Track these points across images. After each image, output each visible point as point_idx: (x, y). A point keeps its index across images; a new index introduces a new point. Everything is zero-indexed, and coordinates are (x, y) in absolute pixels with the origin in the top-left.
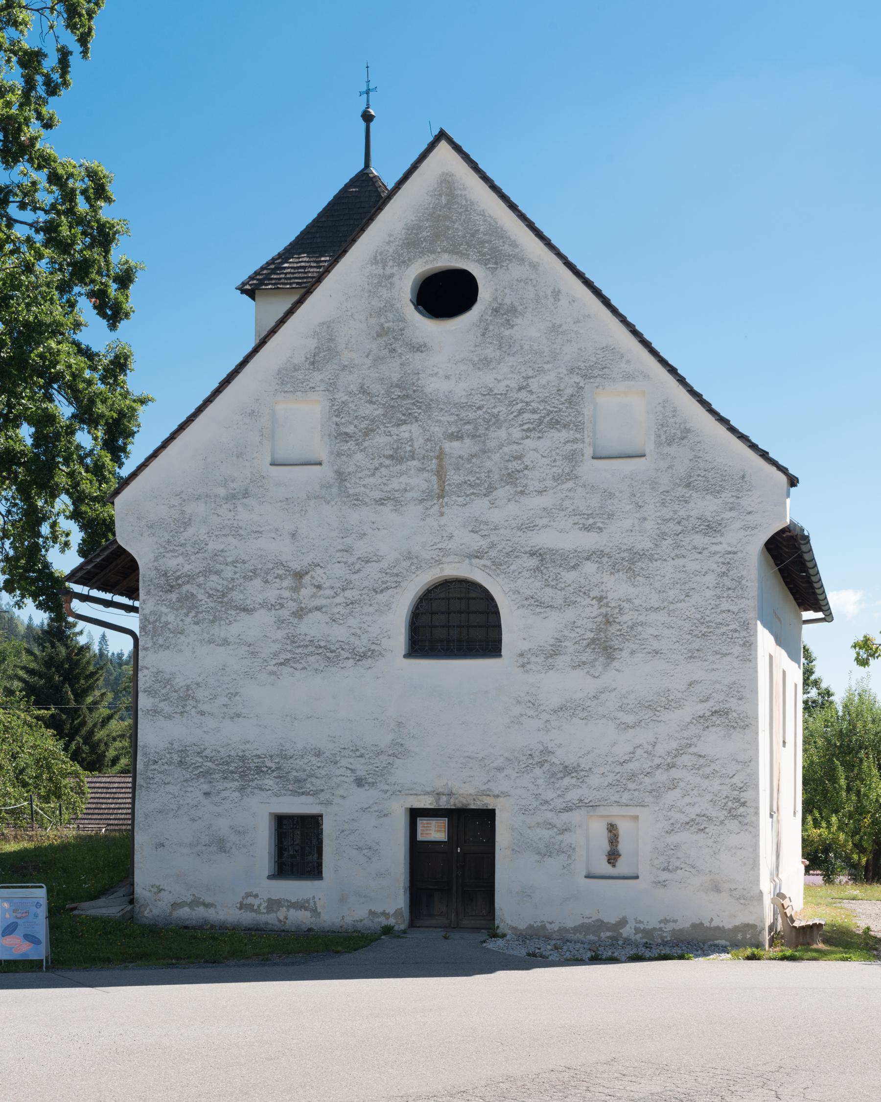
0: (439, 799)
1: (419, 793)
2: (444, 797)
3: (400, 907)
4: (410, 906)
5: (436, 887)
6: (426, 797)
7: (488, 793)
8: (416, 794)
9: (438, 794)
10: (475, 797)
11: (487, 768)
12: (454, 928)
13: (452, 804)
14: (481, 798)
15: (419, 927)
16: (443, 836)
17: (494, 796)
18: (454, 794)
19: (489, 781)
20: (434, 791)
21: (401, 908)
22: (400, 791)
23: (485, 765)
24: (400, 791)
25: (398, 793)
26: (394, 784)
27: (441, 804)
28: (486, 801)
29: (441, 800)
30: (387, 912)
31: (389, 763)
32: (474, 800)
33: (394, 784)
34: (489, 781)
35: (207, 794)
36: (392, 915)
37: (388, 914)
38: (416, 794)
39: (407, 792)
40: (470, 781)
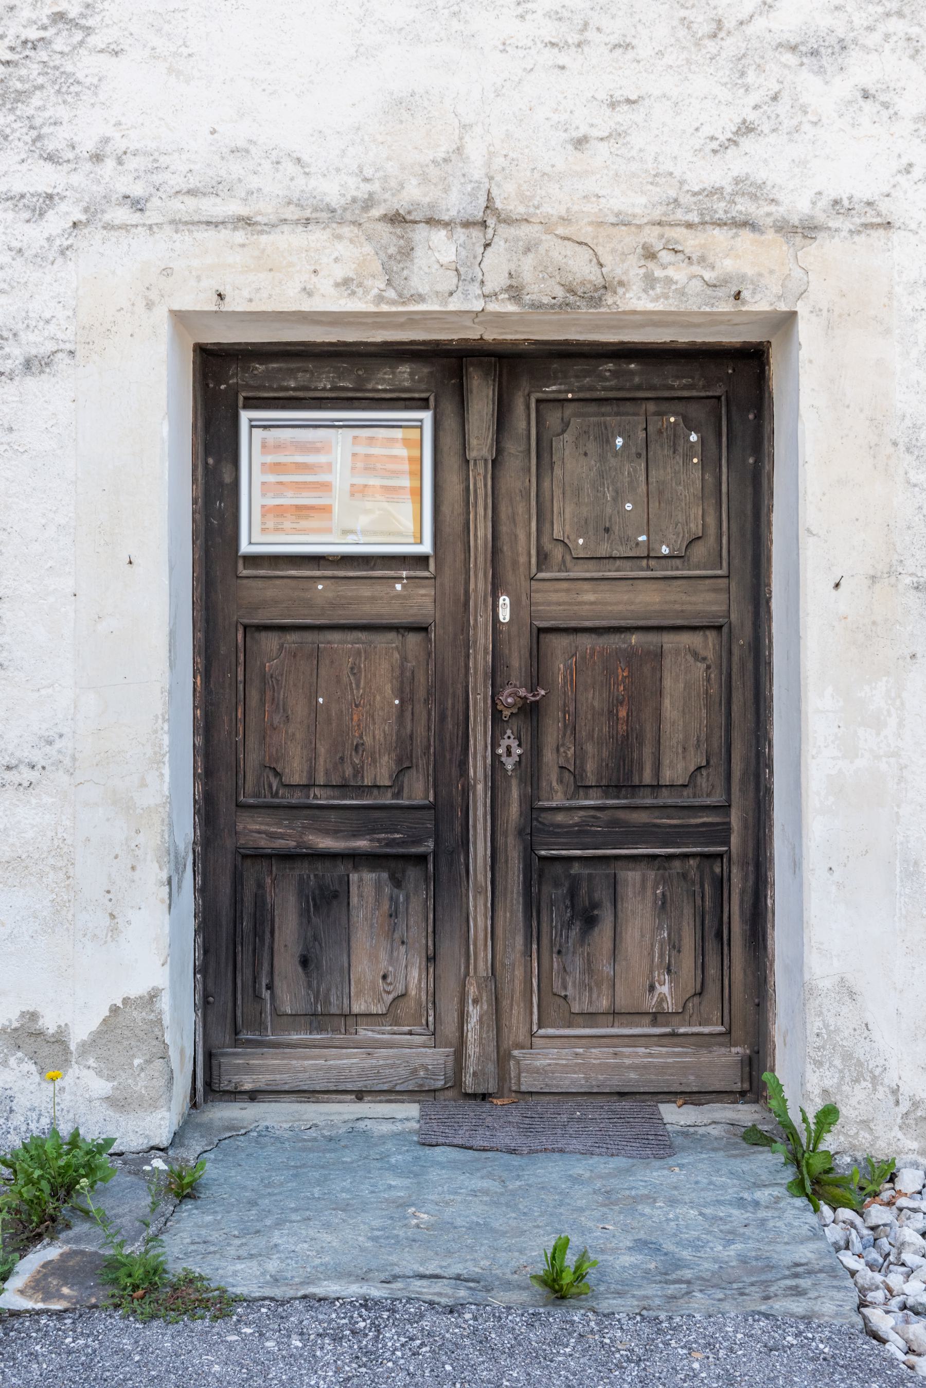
0: (407, 252)
1: (265, 209)
2: (439, 236)
3: (138, 989)
4: (203, 969)
5: (362, 844)
6: (317, 236)
7: (744, 207)
8: (246, 222)
9: (396, 219)
10: (651, 236)
11: (731, 45)
12: (484, 1097)
13: (496, 280)
14: (691, 242)
15: (253, 1096)
16: (407, 523)
17: (785, 229)
18: (507, 221)
19: (747, 129)
20: (369, 203)
21: (153, 996)
22: (138, 205)
23: (718, 29)
24: (138, 205)
25: (122, 215)
26: (97, 158)
27: (419, 283)
28: (728, 265)
29: (421, 257)
30: (49, 1023)
31: (59, 17)
32: (650, 255)
33: (97, 158)
34: (747, 129)
35: (145, 754)
36: (86, 1048)
37: (59, 1041)
38: (246, 222)
39: (188, 206)
40: (615, 135)
